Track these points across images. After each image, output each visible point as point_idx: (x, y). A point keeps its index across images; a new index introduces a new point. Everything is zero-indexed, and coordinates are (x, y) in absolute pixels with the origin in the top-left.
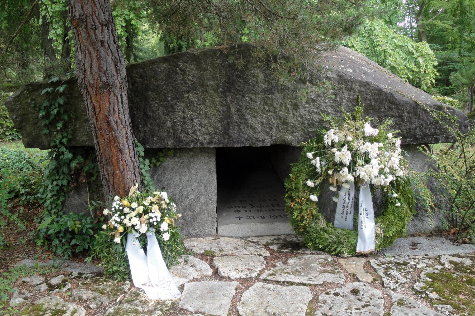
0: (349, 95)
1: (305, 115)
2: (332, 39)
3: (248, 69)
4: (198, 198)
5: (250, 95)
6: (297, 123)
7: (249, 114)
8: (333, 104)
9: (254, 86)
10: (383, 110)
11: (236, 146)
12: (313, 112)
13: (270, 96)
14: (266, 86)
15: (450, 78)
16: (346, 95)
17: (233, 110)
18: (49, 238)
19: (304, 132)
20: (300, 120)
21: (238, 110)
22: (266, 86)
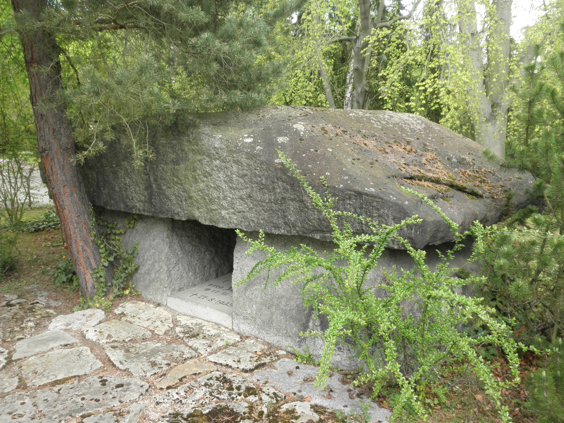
0: (238, 169)
1: (204, 190)
2: (114, 91)
3: (157, 138)
4: (153, 264)
5: (162, 165)
6: (199, 198)
7: (164, 185)
8: (226, 179)
9: (164, 156)
10: (278, 191)
11: (221, 226)
12: (211, 187)
13: (176, 167)
14: (175, 157)
15: (206, 129)
16: (235, 169)
17: (152, 179)
18: (314, 321)
19: (208, 209)
20: (201, 194)
21: (155, 180)
22: (175, 157)
